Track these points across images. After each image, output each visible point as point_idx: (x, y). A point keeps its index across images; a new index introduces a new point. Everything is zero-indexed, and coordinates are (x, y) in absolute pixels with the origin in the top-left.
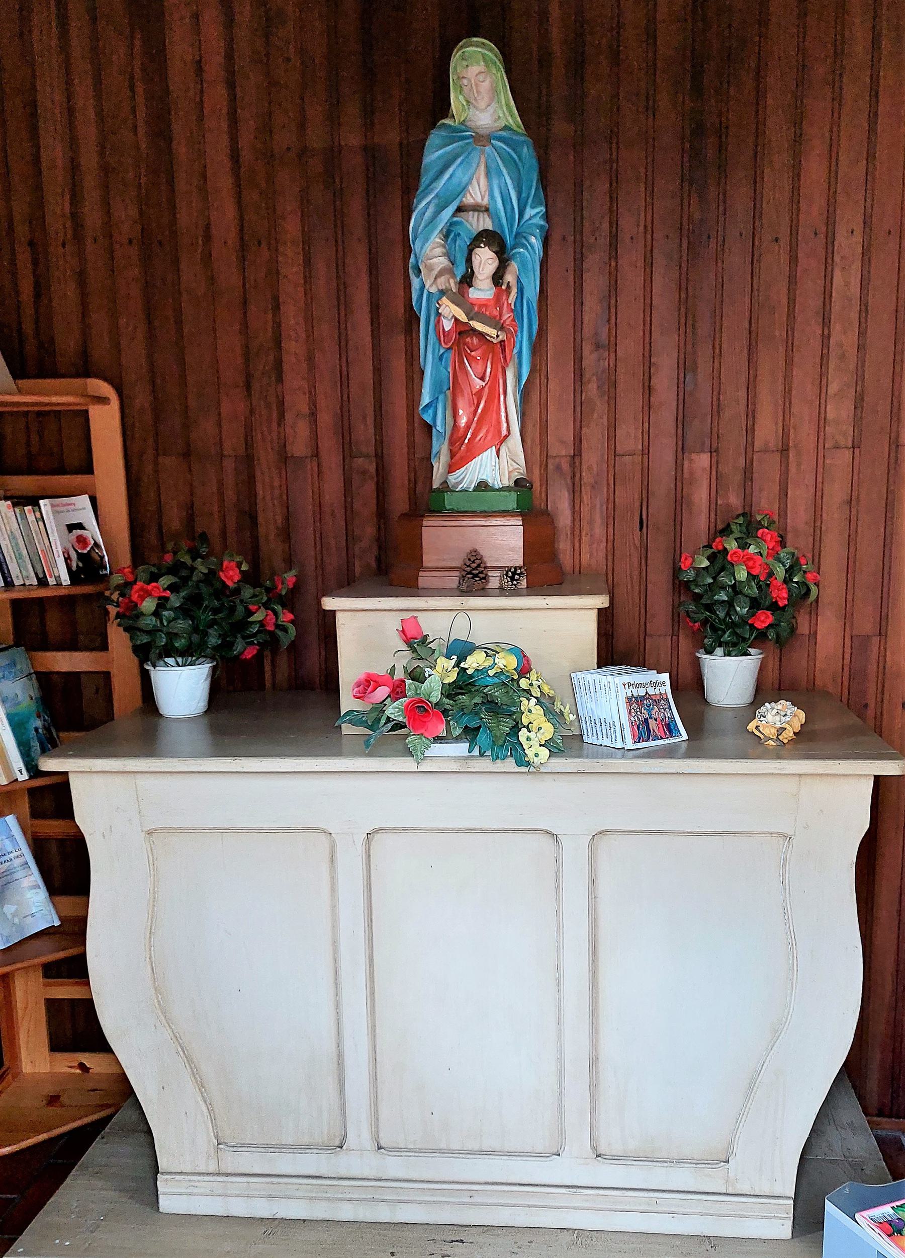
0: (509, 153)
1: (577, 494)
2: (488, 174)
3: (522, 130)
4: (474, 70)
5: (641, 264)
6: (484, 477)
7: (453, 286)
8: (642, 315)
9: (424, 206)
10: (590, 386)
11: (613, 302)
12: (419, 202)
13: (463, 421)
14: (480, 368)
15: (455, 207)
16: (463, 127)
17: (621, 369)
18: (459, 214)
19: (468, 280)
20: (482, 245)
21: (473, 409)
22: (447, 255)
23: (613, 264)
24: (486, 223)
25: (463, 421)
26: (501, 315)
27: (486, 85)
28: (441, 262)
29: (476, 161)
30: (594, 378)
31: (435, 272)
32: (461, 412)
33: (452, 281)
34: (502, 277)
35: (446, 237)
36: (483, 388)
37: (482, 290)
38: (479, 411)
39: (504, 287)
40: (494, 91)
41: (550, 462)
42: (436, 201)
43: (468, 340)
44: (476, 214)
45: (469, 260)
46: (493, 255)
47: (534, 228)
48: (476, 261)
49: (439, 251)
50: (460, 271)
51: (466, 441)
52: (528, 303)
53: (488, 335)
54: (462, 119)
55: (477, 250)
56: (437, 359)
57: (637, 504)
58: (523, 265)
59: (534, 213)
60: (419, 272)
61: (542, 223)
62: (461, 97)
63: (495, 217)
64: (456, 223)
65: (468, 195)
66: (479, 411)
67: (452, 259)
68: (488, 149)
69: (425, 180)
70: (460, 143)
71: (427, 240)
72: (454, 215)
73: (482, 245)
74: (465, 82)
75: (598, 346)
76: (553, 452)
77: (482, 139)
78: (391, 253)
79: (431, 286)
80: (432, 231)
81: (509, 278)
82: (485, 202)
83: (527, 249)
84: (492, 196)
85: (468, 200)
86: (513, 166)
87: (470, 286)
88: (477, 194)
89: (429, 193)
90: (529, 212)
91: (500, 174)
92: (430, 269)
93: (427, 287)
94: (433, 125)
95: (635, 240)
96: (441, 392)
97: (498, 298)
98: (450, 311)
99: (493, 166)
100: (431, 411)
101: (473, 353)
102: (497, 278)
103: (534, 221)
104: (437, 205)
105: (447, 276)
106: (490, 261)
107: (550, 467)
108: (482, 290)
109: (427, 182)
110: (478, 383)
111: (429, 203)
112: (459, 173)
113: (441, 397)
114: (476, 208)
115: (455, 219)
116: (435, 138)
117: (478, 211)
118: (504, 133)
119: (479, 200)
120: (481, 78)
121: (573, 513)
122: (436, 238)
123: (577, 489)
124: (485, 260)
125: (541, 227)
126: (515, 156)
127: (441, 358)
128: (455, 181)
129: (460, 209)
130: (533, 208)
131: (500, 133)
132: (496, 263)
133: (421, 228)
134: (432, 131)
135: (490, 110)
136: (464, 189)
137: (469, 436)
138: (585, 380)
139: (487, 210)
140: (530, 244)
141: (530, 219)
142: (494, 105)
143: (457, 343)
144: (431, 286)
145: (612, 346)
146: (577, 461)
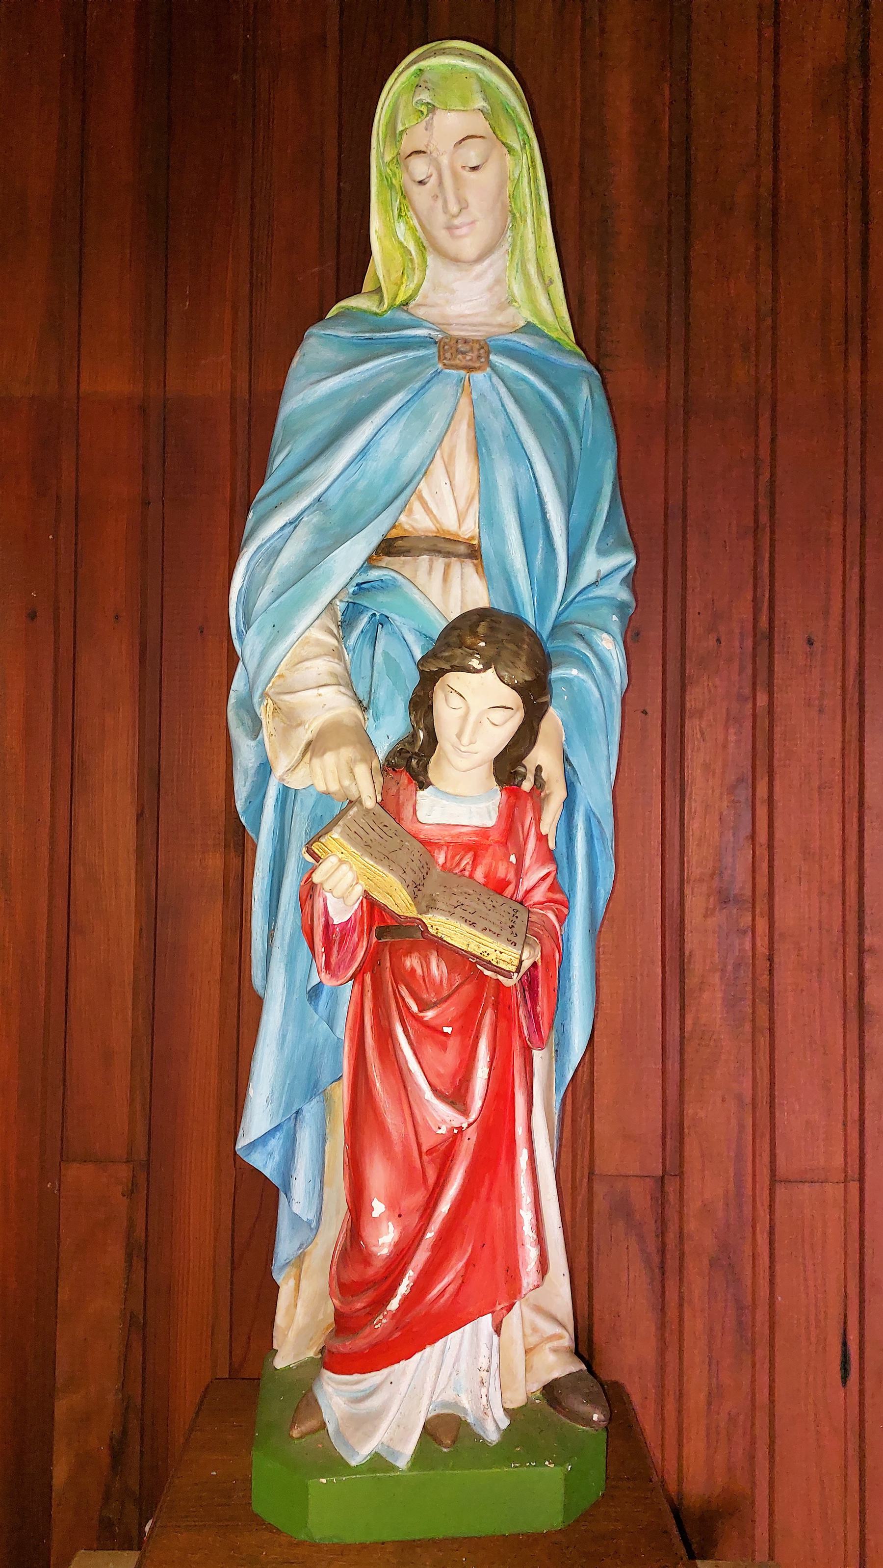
0: (542, 397)
1: (672, 1284)
2: (480, 448)
3: (569, 340)
4: (450, 123)
5: (833, 702)
6: (449, 1396)
7: (366, 787)
8: (838, 826)
9: (276, 535)
10: (706, 995)
11: (762, 790)
12: (262, 520)
13: (384, 1239)
14: (448, 1060)
15: (376, 540)
16: (404, 316)
17: (785, 957)
18: (386, 560)
19: (412, 761)
20: (475, 663)
21: (419, 1197)
22: (347, 682)
23: (762, 700)
24: (461, 592)
25: (384, 1239)
26: (519, 868)
27: (481, 188)
28: (327, 704)
29: (444, 409)
30: (716, 978)
31: (305, 735)
32: (378, 1208)
33: (362, 771)
34: (519, 760)
35: (346, 624)
36: (456, 1136)
37: (459, 799)
38: (444, 1207)
39: (527, 786)
40: (508, 217)
41: (600, 1189)
42: (313, 519)
43: (412, 962)
44: (440, 563)
45: (421, 704)
46: (512, 698)
47: (605, 611)
48: (447, 711)
49: (322, 667)
50: (390, 728)
51: (394, 1305)
52: (588, 821)
53: (489, 965)
54: (400, 298)
55: (454, 679)
56: (300, 994)
57: (835, 1312)
58: (579, 716)
59: (608, 567)
60: (256, 728)
61: (624, 595)
62: (401, 229)
63: (495, 570)
64: (382, 586)
65: (416, 506)
66: (444, 1207)
67: (362, 694)
68: (479, 377)
69: (282, 461)
70: (399, 358)
71: (279, 631)
72: (370, 563)
73: (475, 663)
74: (420, 167)
75: (724, 899)
76: (606, 1164)
77: (462, 353)
78: (184, 657)
79: (293, 769)
80: (298, 605)
81: (543, 756)
82: (469, 529)
83: (586, 666)
84: (489, 515)
85: (417, 521)
86: (557, 433)
87: (423, 785)
88: (445, 503)
89: (297, 493)
90: (593, 565)
91: (520, 453)
92: (290, 720)
93: (280, 768)
94: (320, 316)
95: (817, 645)
96: (313, 1088)
97: (510, 827)
98: (346, 881)
99: (497, 426)
100: (276, 1144)
101: (429, 1015)
102: (508, 766)
103: (602, 591)
104: (321, 530)
105: (347, 753)
106: (498, 716)
107: (601, 1204)
108: (459, 799)
109: (291, 464)
110: (442, 1117)
111: (295, 523)
112: (390, 442)
113: (311, 1110)
114: (443, 546)
115: (374, 574)
116: (318, 346)
117: (448, 554)
118: (526, 341)
119: (450, 522)
120: (472, 154)
121: (662, 1326)
122: (311, 628)
123: (672, 1264)
124: (478, 707)
125: (621, 607)
126: (557, 403)
127: (314, 993)
128: (377, 463)
129: (389, 547)
130: (602, 552)
131: (515, 338)
132: (518, 717)
133: (265, 596)
134: (313, 330)
135: (489, 269)
136: (404, 490)
137: (403, 1289)
138: (691, 981)
139: (474, 553)
140: (596, 655)
141: (595, 584)
142: (498, 260)
143: (372, 963)
144: (293, 769)
145: (764, 897)
146: (671, 1188)
